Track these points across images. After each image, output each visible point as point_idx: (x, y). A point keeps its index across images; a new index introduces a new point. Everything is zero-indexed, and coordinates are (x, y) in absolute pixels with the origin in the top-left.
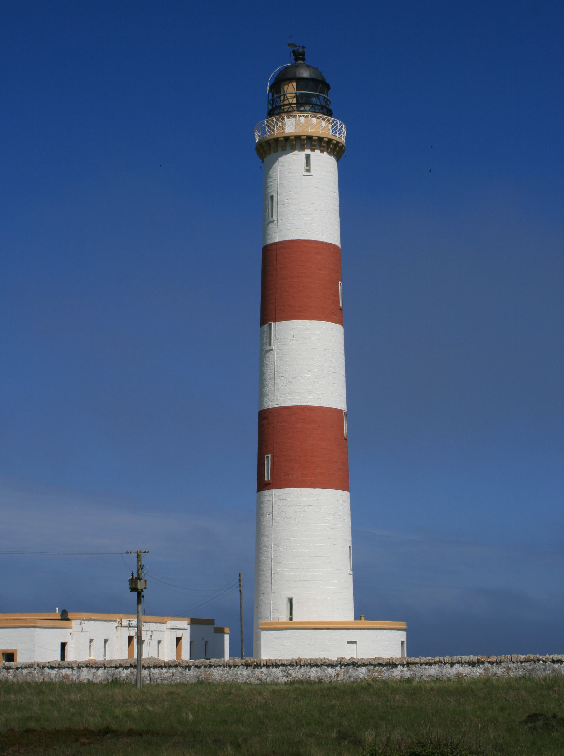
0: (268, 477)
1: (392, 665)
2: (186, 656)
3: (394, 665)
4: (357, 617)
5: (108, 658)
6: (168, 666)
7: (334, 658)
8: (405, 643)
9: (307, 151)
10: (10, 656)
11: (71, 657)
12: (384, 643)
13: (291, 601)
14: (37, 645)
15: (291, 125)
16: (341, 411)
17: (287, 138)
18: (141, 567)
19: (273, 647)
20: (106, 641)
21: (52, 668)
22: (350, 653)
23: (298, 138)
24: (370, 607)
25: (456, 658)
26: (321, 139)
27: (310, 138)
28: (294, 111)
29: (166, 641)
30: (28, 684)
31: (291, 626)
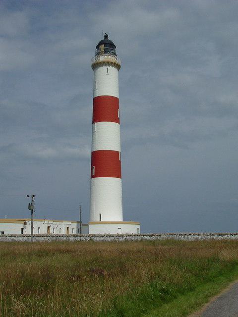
0: (94, 174)
1: (135, 236)
2: (139, 233)
3: (123, 236)
4: (124, 219)
5: (40, 233)
6: (43, 236)
7: (103, 234)
8: (139, 229)
9: (107, 67)
10: (3, 233)
11: (51, 232)
12: (131, 229)
13: (100, 215)
14: (12, 229)
15: (102, 58)
16: (118, 152)
17: (100, 63)
18: (33, 201)
19: (93, 230)
20: (39, 228)
21: (9, 236)
22: (120, 232)
23: (104, 62)
24: (128, 218)
25: (145, 234)
26: (112, 63)
27: (108, 62)
28: (98, 54)
29: (63, 228)
30: (16, 242)
31: (100, 223)
